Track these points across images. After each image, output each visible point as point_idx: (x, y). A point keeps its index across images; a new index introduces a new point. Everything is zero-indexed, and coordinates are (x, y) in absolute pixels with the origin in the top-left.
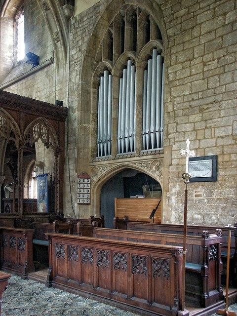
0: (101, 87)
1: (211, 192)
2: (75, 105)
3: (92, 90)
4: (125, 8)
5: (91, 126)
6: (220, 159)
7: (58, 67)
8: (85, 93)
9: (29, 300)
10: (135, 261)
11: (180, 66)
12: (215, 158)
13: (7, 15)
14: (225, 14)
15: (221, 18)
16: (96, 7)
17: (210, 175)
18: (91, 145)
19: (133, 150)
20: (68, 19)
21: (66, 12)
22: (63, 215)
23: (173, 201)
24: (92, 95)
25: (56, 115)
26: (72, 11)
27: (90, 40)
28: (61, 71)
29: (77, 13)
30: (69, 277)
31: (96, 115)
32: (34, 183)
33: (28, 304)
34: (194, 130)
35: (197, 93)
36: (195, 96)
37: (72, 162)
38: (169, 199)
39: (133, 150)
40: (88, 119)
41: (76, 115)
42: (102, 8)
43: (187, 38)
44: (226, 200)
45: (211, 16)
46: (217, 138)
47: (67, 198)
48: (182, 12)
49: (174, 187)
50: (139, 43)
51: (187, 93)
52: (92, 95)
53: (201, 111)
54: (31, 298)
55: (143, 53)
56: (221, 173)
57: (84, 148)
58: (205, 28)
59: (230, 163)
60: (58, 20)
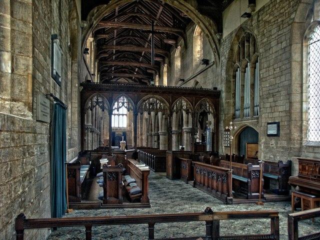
0: (257, 69)
1: (277, 143)
2: (224, 89)
3: (232, 80)
4: (245, 33)
5: (232, 101)
6: (281, 124)
7: (216, 66)
8: (228, 81)
9: (243, 229)
10: (218, 175)
11: (264, 70)
12: (278, 124)
13: (197, 34)
14: (282, 43)
15: (280, 44)
16: (231, 34)
17: (276, 133)
18: (232, 112)
19: (249, 116)
20: (219, 40)
21: (218, 37)
22: (218, 152)
23: (262, 147)
24: (232, 82)
25: (215, 95)
26: (222, 36)
27: (229, 53)
28: (218, 69)
29: (224, 37)
30: (201, 183)
31: (235, 94)
32: (88, 147)
33: (241, 232)
34: (271, 107)
35: (272, 86)
36: (271, 88)
37: (222, 122)
38: (261, 146)
39: (249, 116)
40: (230, 97)
41: (224, 95)
42: (234, 35)
43: (268, 54)
44: (283, 148)
45: (276, 43)
46: (280, 112)
47: (220, 143)
48: (265, 40)
49: (263, 139)
50: (251, 54)
51: (268, 86)
52: (232, 82)
53: (273, 96)
54: (245, 228)
55: (244, 63)
56: (282, 132)
57: (228, 114)
58: (274, 49)
59: (284, 127)
60: (214, 42)
